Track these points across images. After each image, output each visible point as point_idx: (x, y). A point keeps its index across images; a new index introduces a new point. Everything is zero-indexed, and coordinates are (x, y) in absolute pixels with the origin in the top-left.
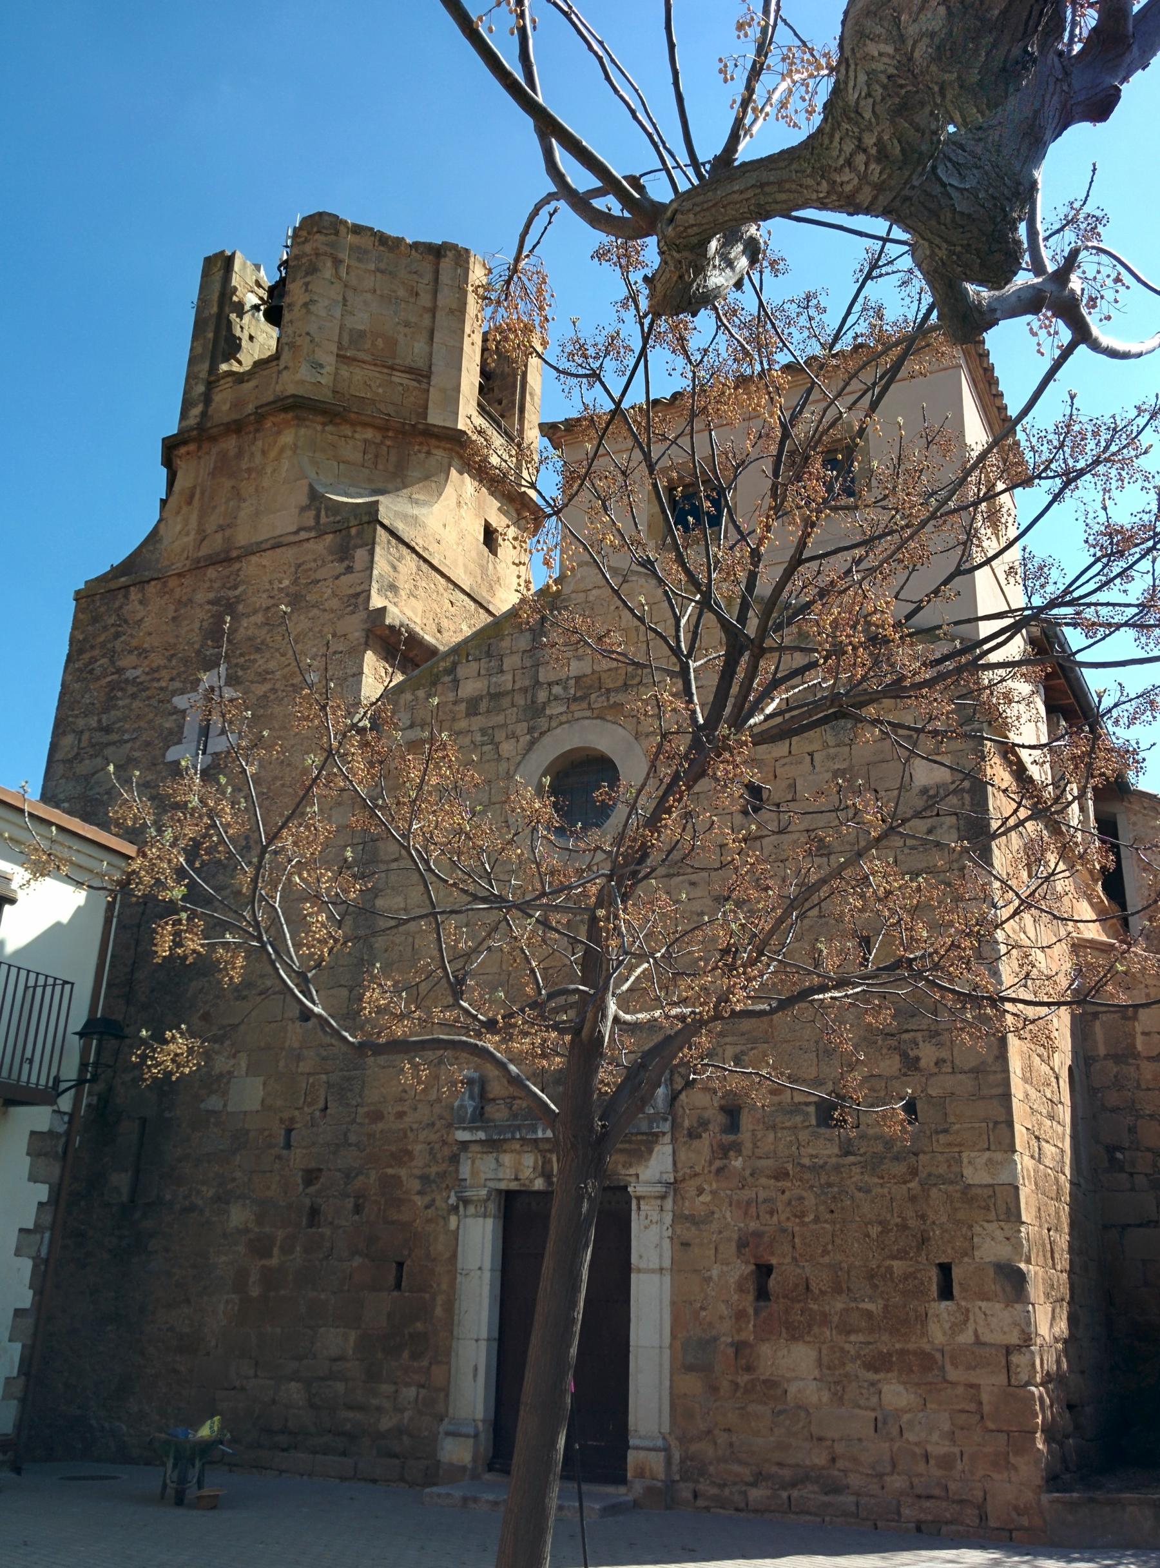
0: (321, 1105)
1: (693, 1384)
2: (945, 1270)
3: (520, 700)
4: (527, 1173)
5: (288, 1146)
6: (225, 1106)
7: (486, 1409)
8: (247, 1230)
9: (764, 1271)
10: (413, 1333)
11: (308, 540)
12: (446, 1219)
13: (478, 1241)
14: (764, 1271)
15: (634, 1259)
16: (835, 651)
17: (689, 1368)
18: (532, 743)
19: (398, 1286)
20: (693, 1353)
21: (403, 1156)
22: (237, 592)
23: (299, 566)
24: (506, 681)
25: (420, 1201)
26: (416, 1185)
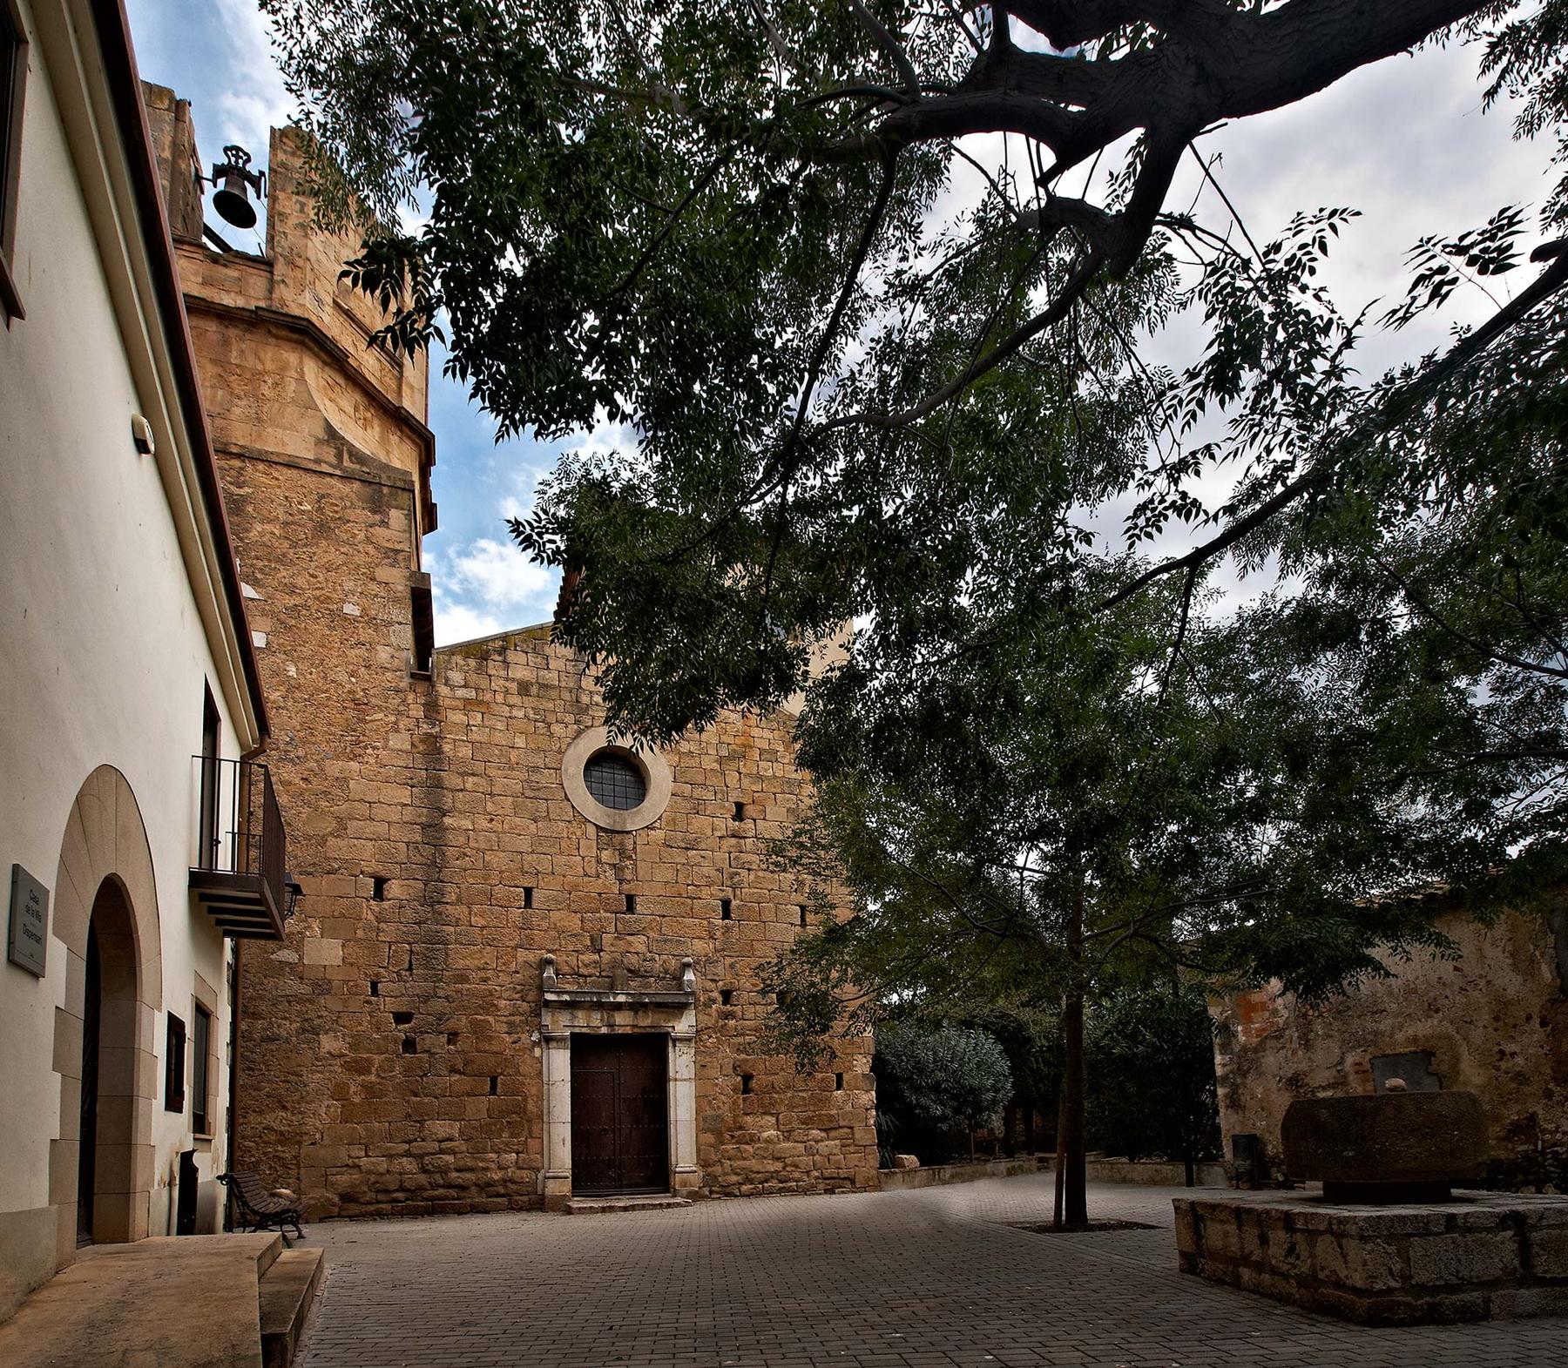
0: (406, 965)
1: (709, 1138)
2: (840, 1076)
3: (566, 696)
4: (597, 1023)
5: (375, 992)
6: (301, 958)
7: (1153, 1182)
8: (342, 1056)
9: (747, 1078)
10: (523, 1119)
11: (331, 475)
12: (532, 1050)
13: (560, 1063)
14: (747, 1078)
15: (671, 1074)
16: (697, 306)
17: (706, 1131)
18: (579, 733)
19: (493, 1090)
20: (707, 1124)
21: (489, 1007)
22: (242, 492)
23: (323, 496)
24: (551, 677)
25: (508, 1038)
26: (505, 1028)
